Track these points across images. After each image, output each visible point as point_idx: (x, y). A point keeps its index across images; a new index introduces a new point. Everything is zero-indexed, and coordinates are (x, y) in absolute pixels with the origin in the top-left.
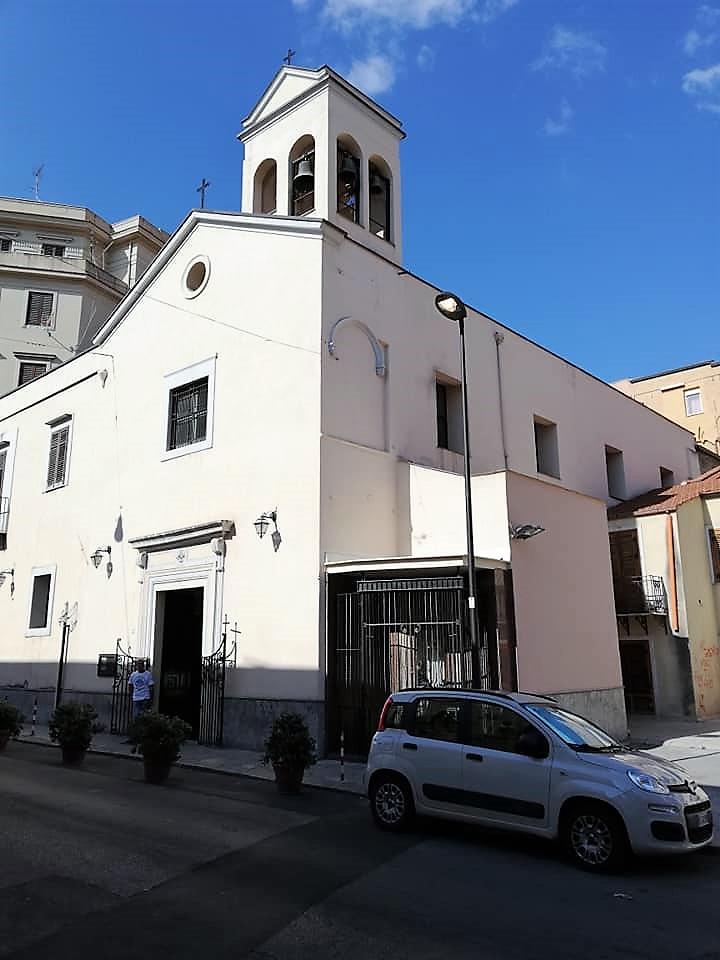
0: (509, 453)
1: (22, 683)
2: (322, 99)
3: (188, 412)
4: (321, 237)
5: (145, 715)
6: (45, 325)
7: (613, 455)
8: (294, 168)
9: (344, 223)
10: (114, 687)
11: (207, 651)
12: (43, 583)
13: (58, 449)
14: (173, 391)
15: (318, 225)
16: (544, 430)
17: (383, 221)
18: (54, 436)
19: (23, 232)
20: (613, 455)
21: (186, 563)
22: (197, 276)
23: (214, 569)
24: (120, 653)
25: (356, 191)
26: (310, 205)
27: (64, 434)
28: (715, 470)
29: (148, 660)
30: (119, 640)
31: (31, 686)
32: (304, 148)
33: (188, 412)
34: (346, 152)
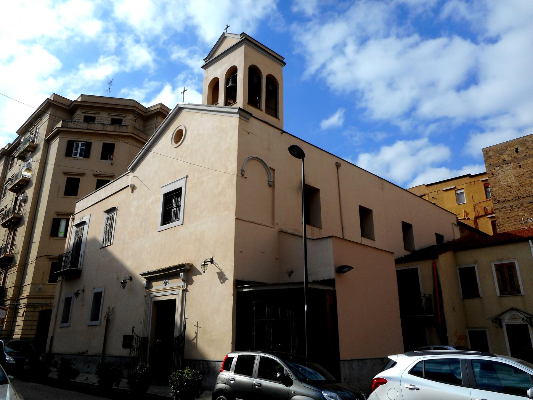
0: (344, 226)
1: (85, 351)
2: (242, 49)
3: (171, 205)
4: (238, 116)
5: (133, 372)
6: (110, 159)
7: (407, 228)
8: (227, 83)
9: (251, 109)
10: (130, 353)
11: (422, 292)
12: (98, 297)
13: (109, 225)
14: (166, 195)
15: (237, 111)
16: (365, 214)
17: (273, 108)
18: (107, 219)
19: (127, 115)
20: (407, 228)
21: (168, 286)
22: (179, 136)
23: (181, 289)
24: (134, 334)
25: (259, 94)
26: (235, 100)
27: (112, 218)
28: (26, 291)
29: (147, 338)
30: (134, 327)
31: (90, 353)
32: (232, 73)
33: (171, 205)
34: (253, 72)
